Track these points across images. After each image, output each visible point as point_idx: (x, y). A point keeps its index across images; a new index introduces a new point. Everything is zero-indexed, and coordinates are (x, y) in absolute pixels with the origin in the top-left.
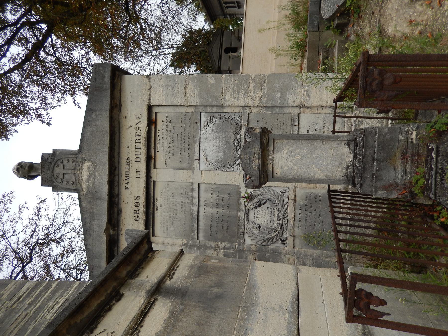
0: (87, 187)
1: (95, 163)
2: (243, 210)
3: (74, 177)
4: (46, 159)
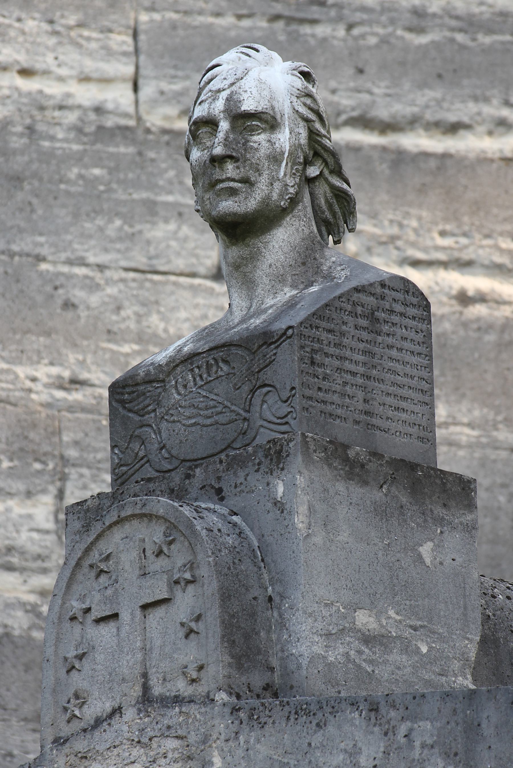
3: (108, 707)
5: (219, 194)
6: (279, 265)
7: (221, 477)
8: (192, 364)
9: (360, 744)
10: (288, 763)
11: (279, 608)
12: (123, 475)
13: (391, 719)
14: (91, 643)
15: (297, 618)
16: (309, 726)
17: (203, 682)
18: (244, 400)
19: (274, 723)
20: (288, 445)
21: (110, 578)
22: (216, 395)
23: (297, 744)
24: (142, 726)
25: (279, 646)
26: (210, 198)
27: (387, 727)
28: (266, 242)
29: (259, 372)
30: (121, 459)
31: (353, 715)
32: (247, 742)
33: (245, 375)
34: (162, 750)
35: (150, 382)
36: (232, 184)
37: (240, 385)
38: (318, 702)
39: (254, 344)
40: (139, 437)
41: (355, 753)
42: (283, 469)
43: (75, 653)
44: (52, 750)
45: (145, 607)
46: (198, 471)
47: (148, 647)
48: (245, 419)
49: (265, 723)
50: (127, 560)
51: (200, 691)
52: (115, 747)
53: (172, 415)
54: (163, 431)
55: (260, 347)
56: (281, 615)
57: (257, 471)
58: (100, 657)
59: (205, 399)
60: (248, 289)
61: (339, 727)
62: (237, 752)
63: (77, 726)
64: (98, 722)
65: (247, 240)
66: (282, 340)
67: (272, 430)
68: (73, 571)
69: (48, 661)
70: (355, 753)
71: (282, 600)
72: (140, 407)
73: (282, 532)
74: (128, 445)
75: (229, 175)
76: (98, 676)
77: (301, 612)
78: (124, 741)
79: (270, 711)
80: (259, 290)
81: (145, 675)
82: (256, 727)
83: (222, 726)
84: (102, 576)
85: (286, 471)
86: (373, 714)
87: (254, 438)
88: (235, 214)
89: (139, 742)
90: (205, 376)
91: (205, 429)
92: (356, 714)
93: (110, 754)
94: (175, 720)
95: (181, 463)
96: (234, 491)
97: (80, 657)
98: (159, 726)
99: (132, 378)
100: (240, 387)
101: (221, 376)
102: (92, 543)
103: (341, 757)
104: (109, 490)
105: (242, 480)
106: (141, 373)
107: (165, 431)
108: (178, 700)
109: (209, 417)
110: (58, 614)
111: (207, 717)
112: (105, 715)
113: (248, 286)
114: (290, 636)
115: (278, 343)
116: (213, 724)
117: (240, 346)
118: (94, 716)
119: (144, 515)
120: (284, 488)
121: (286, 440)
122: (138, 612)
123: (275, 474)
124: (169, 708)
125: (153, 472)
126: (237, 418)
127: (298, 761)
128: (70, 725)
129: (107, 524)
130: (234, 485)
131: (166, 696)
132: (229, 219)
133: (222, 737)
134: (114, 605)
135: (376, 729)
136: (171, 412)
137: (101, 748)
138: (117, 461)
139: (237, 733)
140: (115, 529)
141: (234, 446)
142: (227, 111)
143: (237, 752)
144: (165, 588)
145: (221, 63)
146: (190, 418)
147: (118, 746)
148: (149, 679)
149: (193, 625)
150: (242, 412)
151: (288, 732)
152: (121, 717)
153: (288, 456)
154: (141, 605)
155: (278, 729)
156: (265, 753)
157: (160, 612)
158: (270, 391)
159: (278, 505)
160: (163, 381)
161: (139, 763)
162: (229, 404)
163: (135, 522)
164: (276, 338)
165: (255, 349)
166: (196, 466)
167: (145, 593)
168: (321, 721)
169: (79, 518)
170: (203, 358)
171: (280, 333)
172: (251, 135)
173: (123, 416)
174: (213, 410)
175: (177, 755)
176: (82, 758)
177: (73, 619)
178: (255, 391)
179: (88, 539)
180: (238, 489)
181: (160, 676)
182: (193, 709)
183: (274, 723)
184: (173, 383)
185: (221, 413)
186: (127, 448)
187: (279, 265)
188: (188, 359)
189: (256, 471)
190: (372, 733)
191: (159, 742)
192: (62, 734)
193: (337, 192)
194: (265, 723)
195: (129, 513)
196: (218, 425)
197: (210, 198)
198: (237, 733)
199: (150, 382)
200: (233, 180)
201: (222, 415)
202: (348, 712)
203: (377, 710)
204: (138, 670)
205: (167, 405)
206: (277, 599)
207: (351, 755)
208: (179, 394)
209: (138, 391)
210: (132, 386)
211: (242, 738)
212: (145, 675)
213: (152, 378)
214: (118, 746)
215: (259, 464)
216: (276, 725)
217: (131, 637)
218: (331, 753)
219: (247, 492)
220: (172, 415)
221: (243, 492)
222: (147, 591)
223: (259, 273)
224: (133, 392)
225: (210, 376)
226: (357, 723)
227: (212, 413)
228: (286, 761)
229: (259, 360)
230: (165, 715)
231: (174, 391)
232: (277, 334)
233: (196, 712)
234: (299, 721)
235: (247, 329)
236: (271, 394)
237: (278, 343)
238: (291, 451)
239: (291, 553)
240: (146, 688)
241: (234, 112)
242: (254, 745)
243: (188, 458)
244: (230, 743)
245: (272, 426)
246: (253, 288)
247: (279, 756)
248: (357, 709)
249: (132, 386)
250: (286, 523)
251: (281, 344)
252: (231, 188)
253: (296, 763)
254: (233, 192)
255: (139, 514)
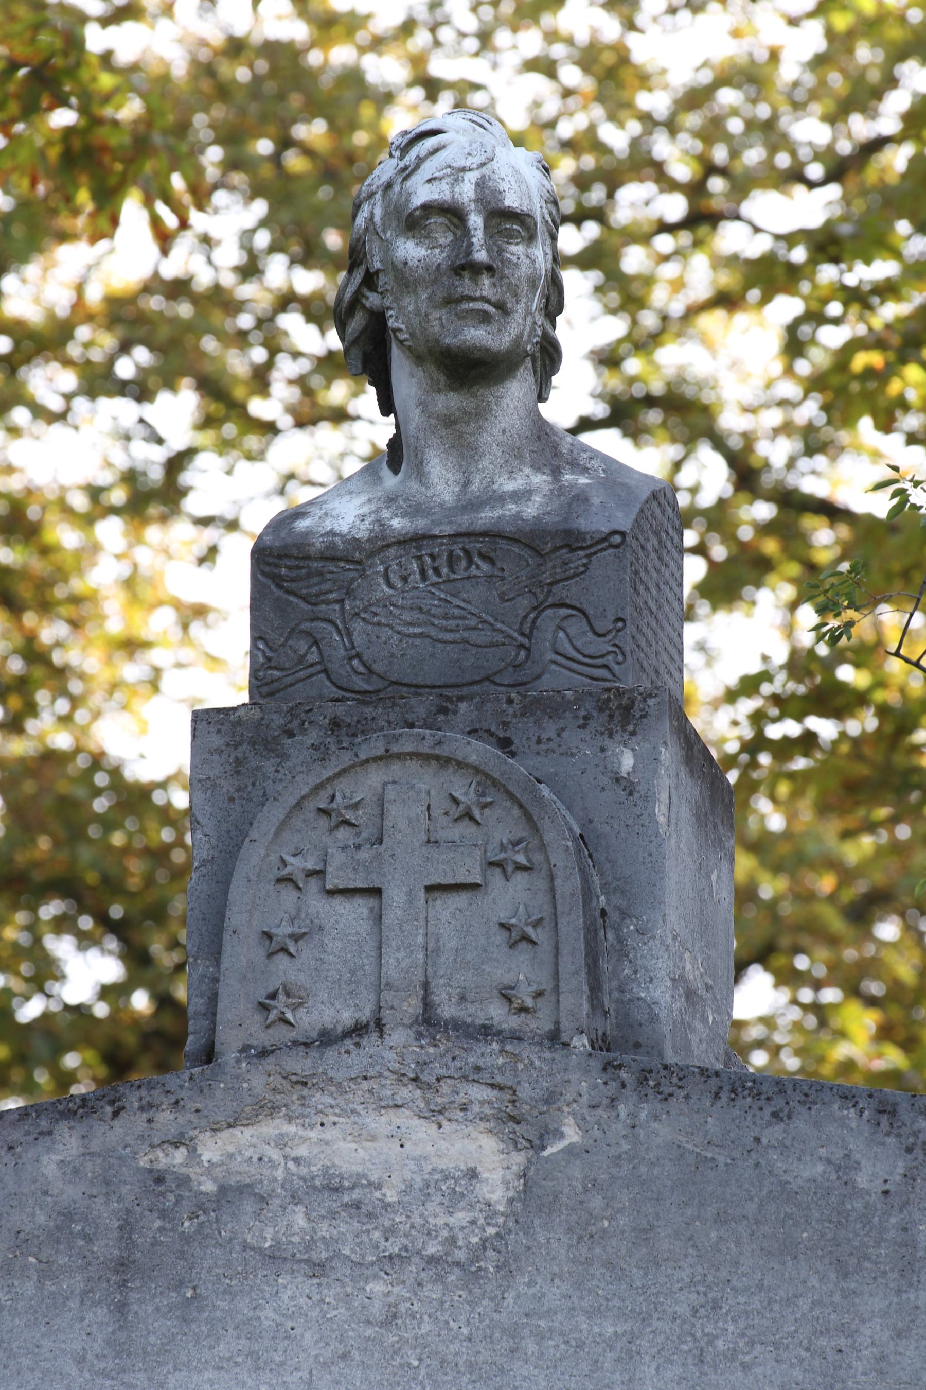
0: (244, 1189)
1: (506, 1269)
2: (814, 443)
3: (347, 1017)
4: (571, 591)
5: (463, 316)
6: (514, 432)
7: (509, 723)
8: (419, 548)
9: (857, 1156)
10: (713, 1159)
11: (617, 929)
12: (272, 682)
13: (919, 1131)
14: (316, 921)
15: (651, 949)
16: (758, 1113)
17: (540, 1014)
18: (520, 619)
19: (687, 1097)
20: (645, 700)
21: (358, 834)
22: (464, 601)
23: (732, 1134)
24: (425, 1058)
25: (615, 984)
26: (440, 318)
27: (911, 1140)
28: (498, 397)
29: (551, 584)
30: (269, 659)
31: (845, 1112)
32: (633, 1115)
33: (523, 584)
34: (461, 1099)
35: (334, 559)
36: (487, 307)
37: (511, 596)
38: (777, 1083)
39: (546, 543)
40: (309, 634)
41: (846, 1167)
42: (633, 733)
43: (289, 930)
44: (238, 1061)
45: (429, 889)
46: (463, 706)
47: (431, 946)
48: (522, 646)
49: (671, 1095)
50: (403, 816)
51: (532, 1026)
52: (365, 1078)
53: (376, 614)
54: (355, 633)
55: (556, 549)
56: (620, 940)
57: (583, 727)
58: (333, 945)
59: (443, 604)
60: (462, 456)
61: (818, 1125)
62: (614, 1126)
63: (281, 1034)
64: (327, 1039)
65: (474, 389)
66: (599, 547)
67: (579, 674)
68: (290, 812)
69: (234, 932)
70: (846, 1167)
71: (624, 919)
72: (315, 590)
73: (629, 823)
74: (286, 641)
75: (485, 293)
76: (328, 971)
77: (658, 942)
78: (386, 1073)
79: (680, 1079)
80: (485, 462)
81: (426, 985)
82: (651, 1097)
83: (584, 1084)
84: (341, 829)
85: (639, 737)
86: (884, 1120)
87: (539, 677)
88: (487, 350)
89: (415, 1079)
90: (445, 571)
91: (440, 645)
92: (852, 1113)
93: (353, 1087)
94: (489, 1061)
95: (389, 686)
96: (535, 748)
97: (296, 938)
98: (458, 1064)
99: (298, 548)
100: (513, 599)
101: (475, 576)
102: (329, 780)
103: (820, 1168)
104: (247, 701)
105: (553, 735)
106: (318, 544)
107: (359, 635)
108: (486, 1032)
109: (451, 631)
110: (257, 869)
111: (554, 1066)
112: (340, 1029)
113: (462, 453)
114: (635, 972)
115: (592, 551)
116: (566, 1078)
117: (517, 541)
118: (319, 1027)
119: (437, 758)
120: (636, 760)
121: (641, 694)
122: (422, 894)
123: (617, 737)
124: (478, 1040)
125: (334, 689)
126: (506, 641)
127: (733, 1160)
128: (271, 1031)
129: (363, 756)
130: (535, 739)
131: (464, 1023)
132: (477, 354)
133: (585, 1100)
134: (374, 876)
135: (891, 1140)
136: (374, 609)
137: (339, 1075)
138: (261, 660)
139: (613, 1100)
140: (373, 767)
141: (497, 679)
142: (480, 200)
143: (614, 1126)
144: (477, 869)
145: (445, 128)
146: (411, 624)
147: (372, 1077)
148: (433, 993)
149: (530, 930)
150: (515, 635)
151: (715, 1115)
152: (381, 1037)
153: (644, 716)
154: (427, 884)
155: (695, 1107)
156: (669, 1137)
157: (459, 900)
158: (572, 615)
159: (623, 783)
160: (359, 562)
161: (409, 1108)
162: (491, 620)
163: (413, 765)
164: (589, 542)
165: (547, 550)
166: (461, 699)
167: (436, 869)
168: (781, 1110)
169: (219, 731)
170: (442, 544)
171: (598, 536)
172: (508, 243)
173: (278, 599)
174: (460, 622)
175: (487, 1110)
176: (297, 1082)
177: (288, 880)
178: (543, 610)
179: (324, 772)
180: (544, 747)
181: (454, 992)
182: (527, 1051)
183: (687, 1097)
184: (381, 568)
185: (475, 628)
186: (283, 645)
187: (514, 432)
188: (412, 540)
189: (579, 727)
190: (883, 1144)
191: (455, 1086)
192: (254, 1042)
193: (545, 344)
194: (671, 1095)
195: (409, 748)
196: (467, 646)
197: (440, 318)
198: (613, 1100)
199: (334, 559)
200: (488, 301)
201: (476, 633)
202: (836, 1106)
203: (893, 1113)
204: (419, 977)
205: (366, 598)
206: (614, 916)
207: (838, 1168)
208: (390, 585)
209: (308, 567)
210: (296, 558)
211: (622, 1109)
212: (426, 985)
213: (339, 554)
214: (372, 1077)
215: (586, 718)
216: (692, 1101)
217: (406, 927)
218: (799, 1160)
219: (561, 754)
220: (376, 614)
221: (554, 752)
222: (442, 867)
223: (486, 438)
224: (298, 568)
225: (453, 572)
226: (854, 1125)
227: (458, 626)
228: (709, 1155)
229: (554, 567)
230: (471, 1049)
231: (381, 580)
232: (592, 538)
233: (534, 1057)
234: (738, 1103)
235: (518, 516)
236: (573, 619)
237: (592, 551)
238: (651, 711)
239: (646, 855)
240: (427, 1005)
241: (493, 205)
242: (647, 1122)
243: (405, 681)
244: (599, 1111)
245: (575, 666)
246: (472, 457)
247: (695, 1145)
248: (854, 1106)
249: (296, 558)
250: (637, 811)
251: (595, 553)
252: (485, 312)
253: (729, 1161)
254: (485, 318)
255: (427, 754)
